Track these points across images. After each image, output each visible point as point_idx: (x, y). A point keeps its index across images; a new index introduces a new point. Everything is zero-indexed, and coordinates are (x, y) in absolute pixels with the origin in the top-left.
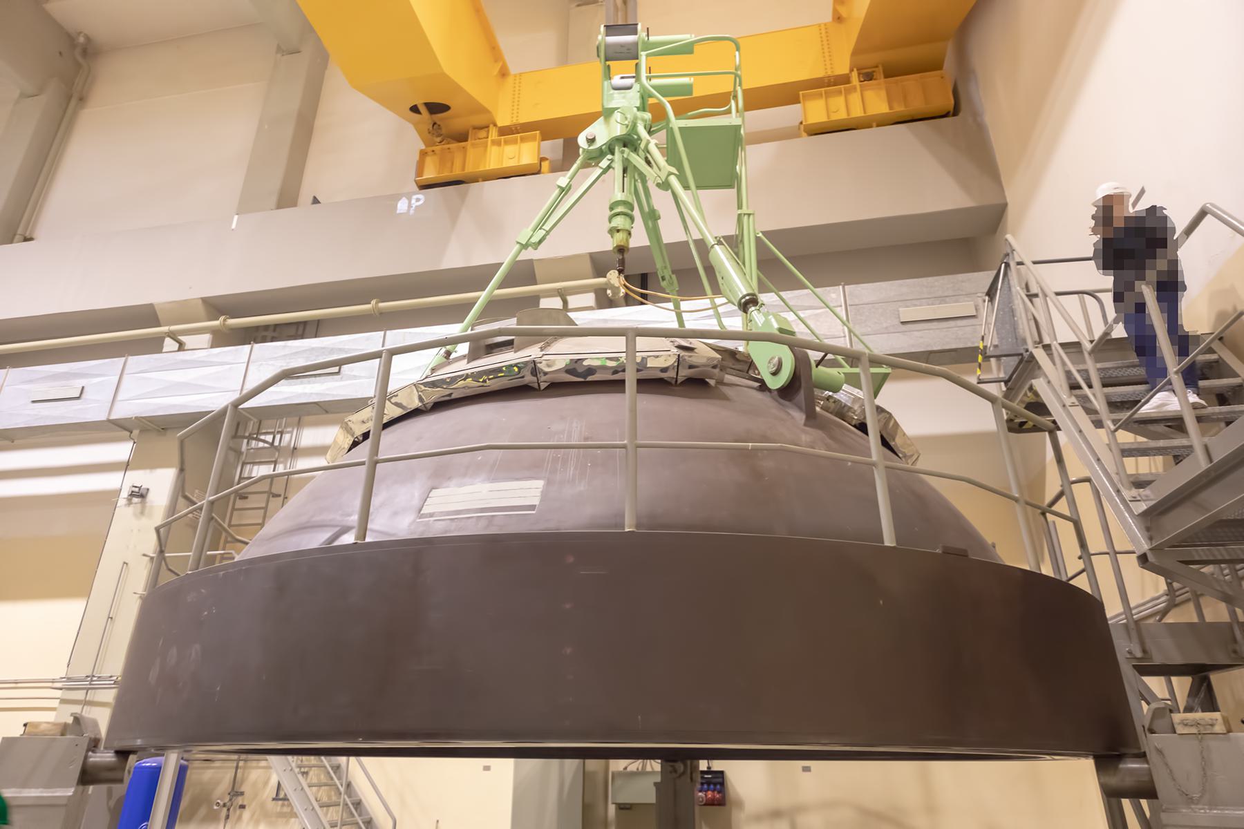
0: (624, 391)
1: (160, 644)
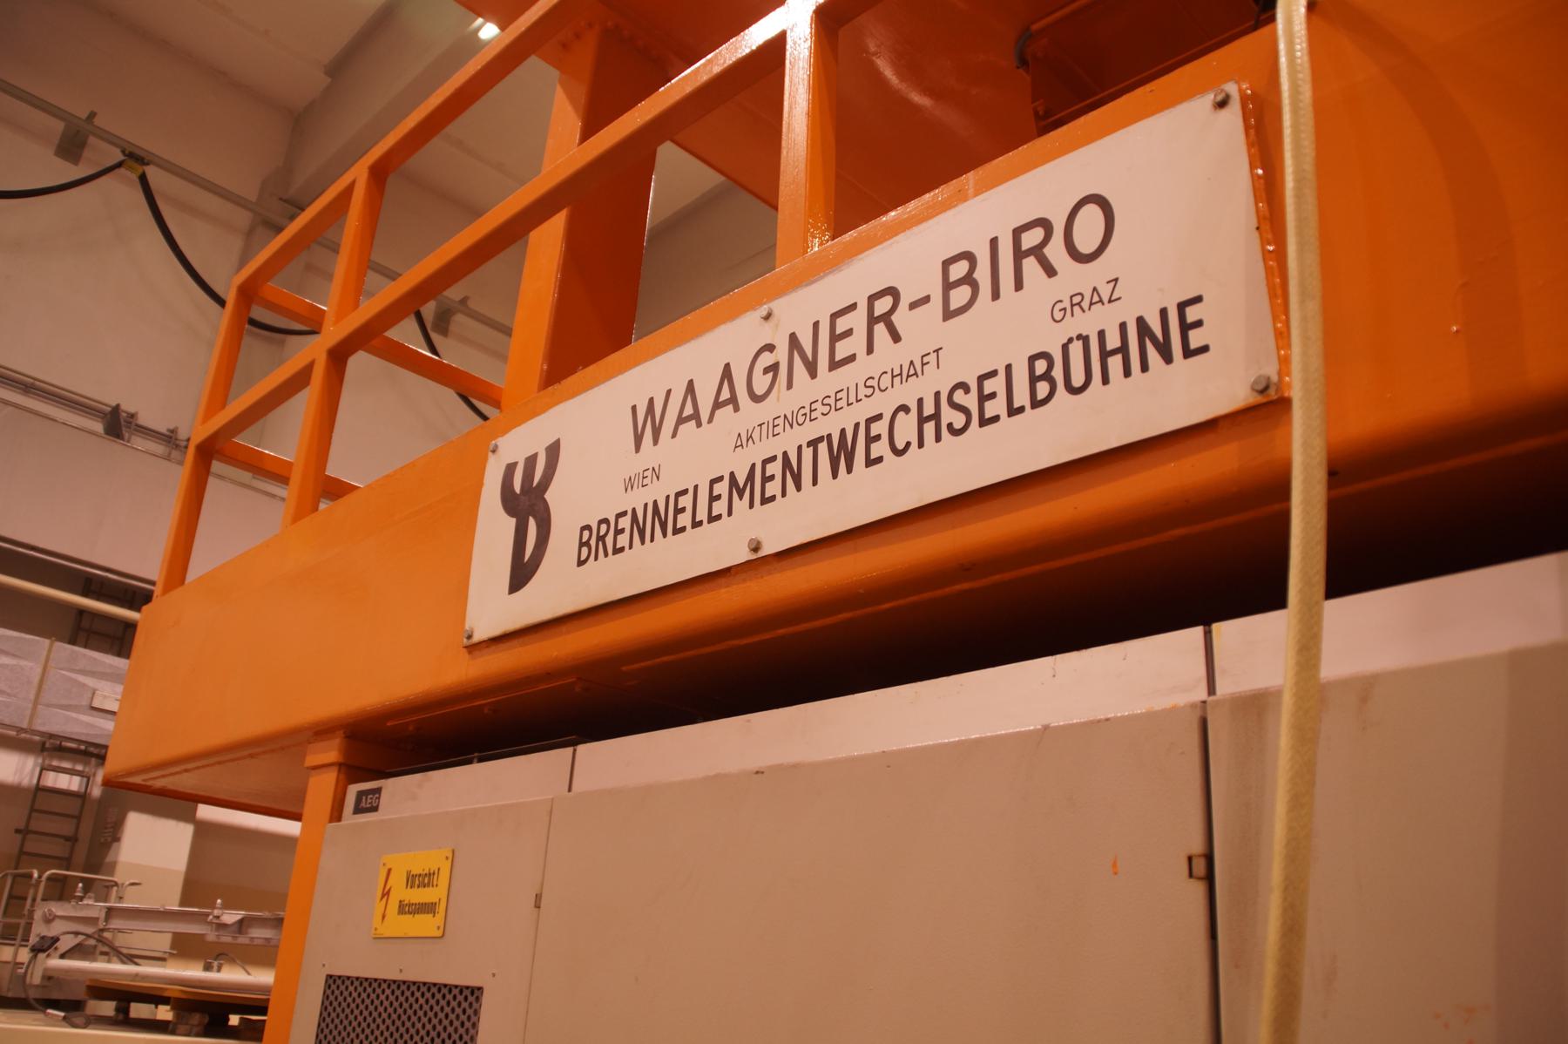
1: (663, 88)
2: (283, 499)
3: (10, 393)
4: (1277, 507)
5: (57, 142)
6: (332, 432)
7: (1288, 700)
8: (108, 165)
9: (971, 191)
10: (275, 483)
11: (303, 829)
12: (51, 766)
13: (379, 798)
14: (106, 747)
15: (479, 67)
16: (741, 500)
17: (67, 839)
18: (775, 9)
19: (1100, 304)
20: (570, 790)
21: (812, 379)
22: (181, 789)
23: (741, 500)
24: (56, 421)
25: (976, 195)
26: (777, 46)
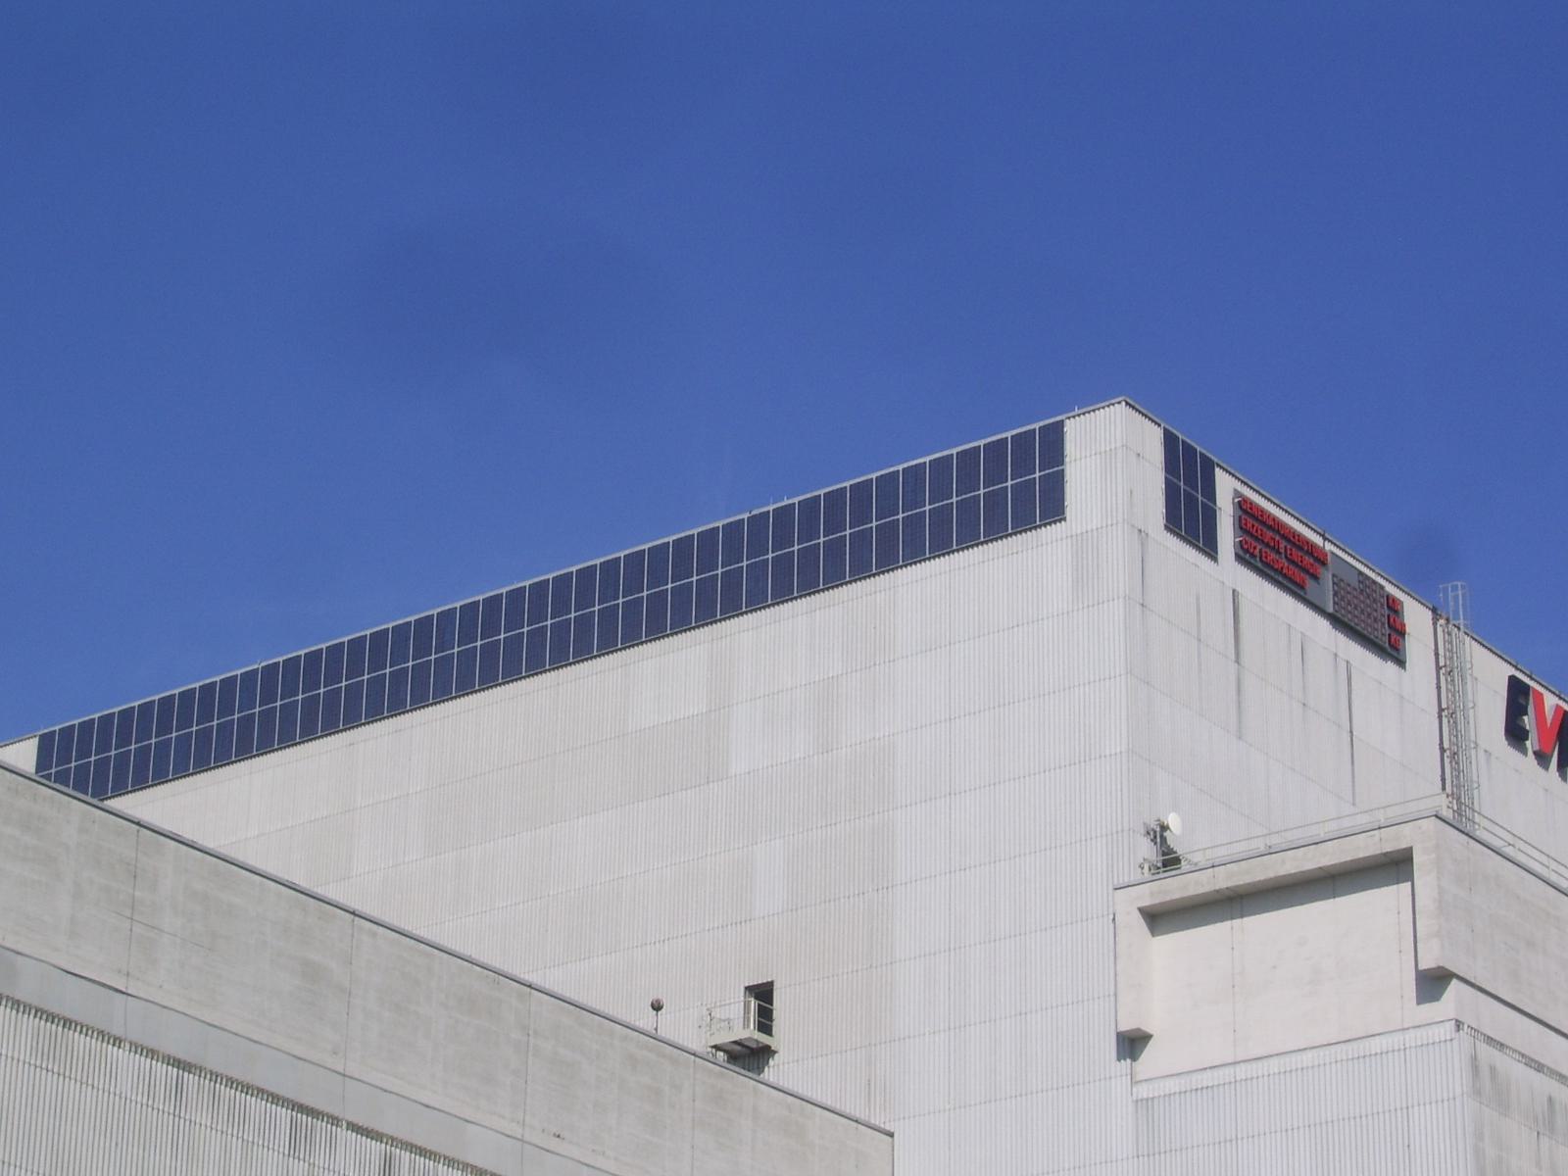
0: (1409, 877)
2: (1143, 874)
3: (1176, 895)
4: (1060, 468)
5: (1395, 886)
6: (1561, 724)
7: (761, 1003)
8: (1484, 986)
9: (763, 1020)
10: (737, 1069)
11: (1091, 397)
12: (1315, 560)
13: (1548, 1068)
14: (1153, 934)
15: (1241, 883)
16: (1401, 663)
17: (1137, 1082)
18: (1216, 922)
19: (1157, 860)
20: (1395, 866)
21: (746, 988)
22: (248, 865)
23: (1401, 663)
24: (1414, 1027)
25: (1166, 478)
26: (1244, 508)
